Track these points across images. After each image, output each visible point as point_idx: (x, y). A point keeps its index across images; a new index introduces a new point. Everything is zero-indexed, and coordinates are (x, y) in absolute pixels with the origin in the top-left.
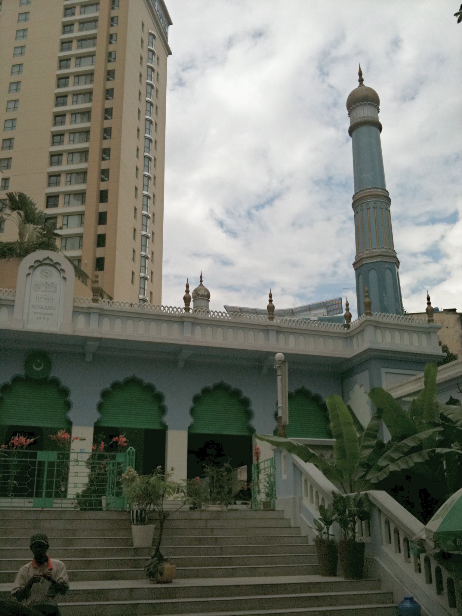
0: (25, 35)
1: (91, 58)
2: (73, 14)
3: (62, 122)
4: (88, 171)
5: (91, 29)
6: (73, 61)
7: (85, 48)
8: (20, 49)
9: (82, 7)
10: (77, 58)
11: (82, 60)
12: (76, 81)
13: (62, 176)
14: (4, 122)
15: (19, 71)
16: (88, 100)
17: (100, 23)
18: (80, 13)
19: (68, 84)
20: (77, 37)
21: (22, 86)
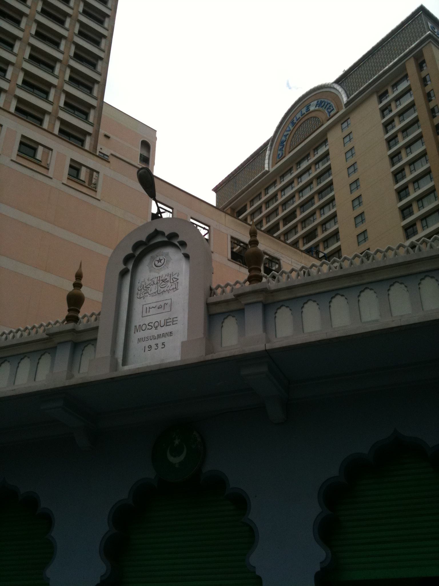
0: (361, 201)
1: (432, 194)
2: (391, 111)
3: (414, 233)
4: (423, 134)
5: (415, 131)
6: (415, 206)
7: (411, 134)
8: (363, 235)
9: (422, 220)
10: (422, 220)
11: (428, 219)
12: (425, 224)
13: (405, 169)
14: (347, 170)
15: (362, 220)
16: (430, 180)
17: (421, 122)
18: (423, 228)
19: (417, 231)
20: (400, 129)
21: (366, 216)
